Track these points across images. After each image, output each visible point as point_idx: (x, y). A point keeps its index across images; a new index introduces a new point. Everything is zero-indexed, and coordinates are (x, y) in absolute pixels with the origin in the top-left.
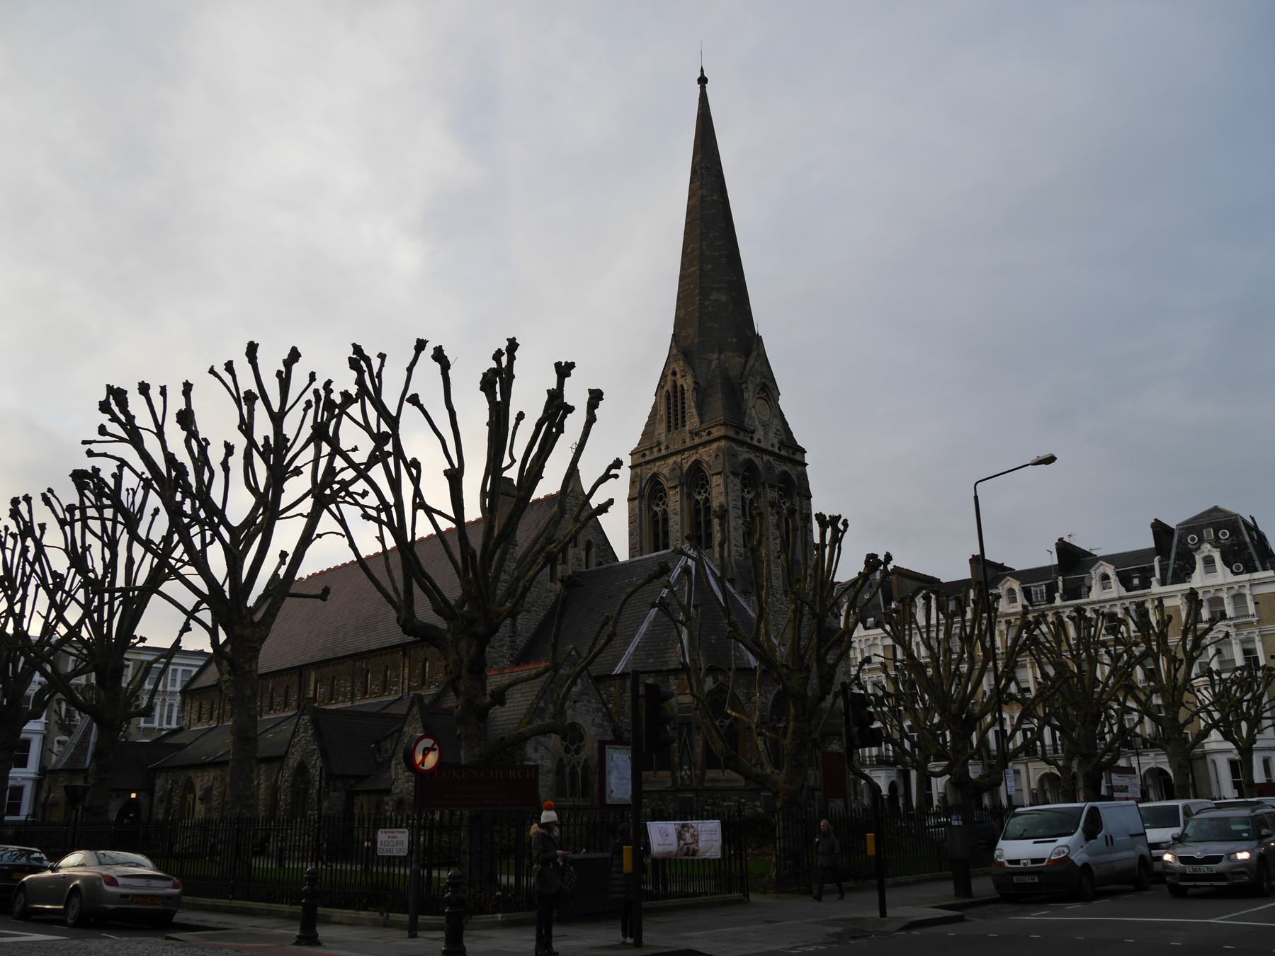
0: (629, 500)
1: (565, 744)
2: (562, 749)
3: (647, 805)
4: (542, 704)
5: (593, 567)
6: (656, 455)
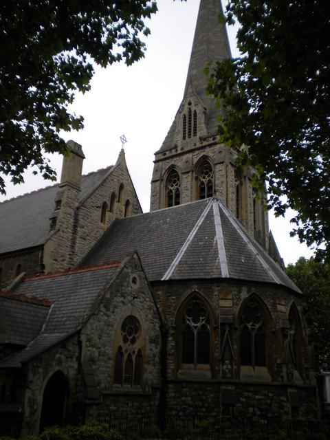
0: (153, 182)
1: (124, 334)
2: (121, 338)
3: (188, 394)
4: (108, 296)
5: (130, 216)
6: (174, 153)
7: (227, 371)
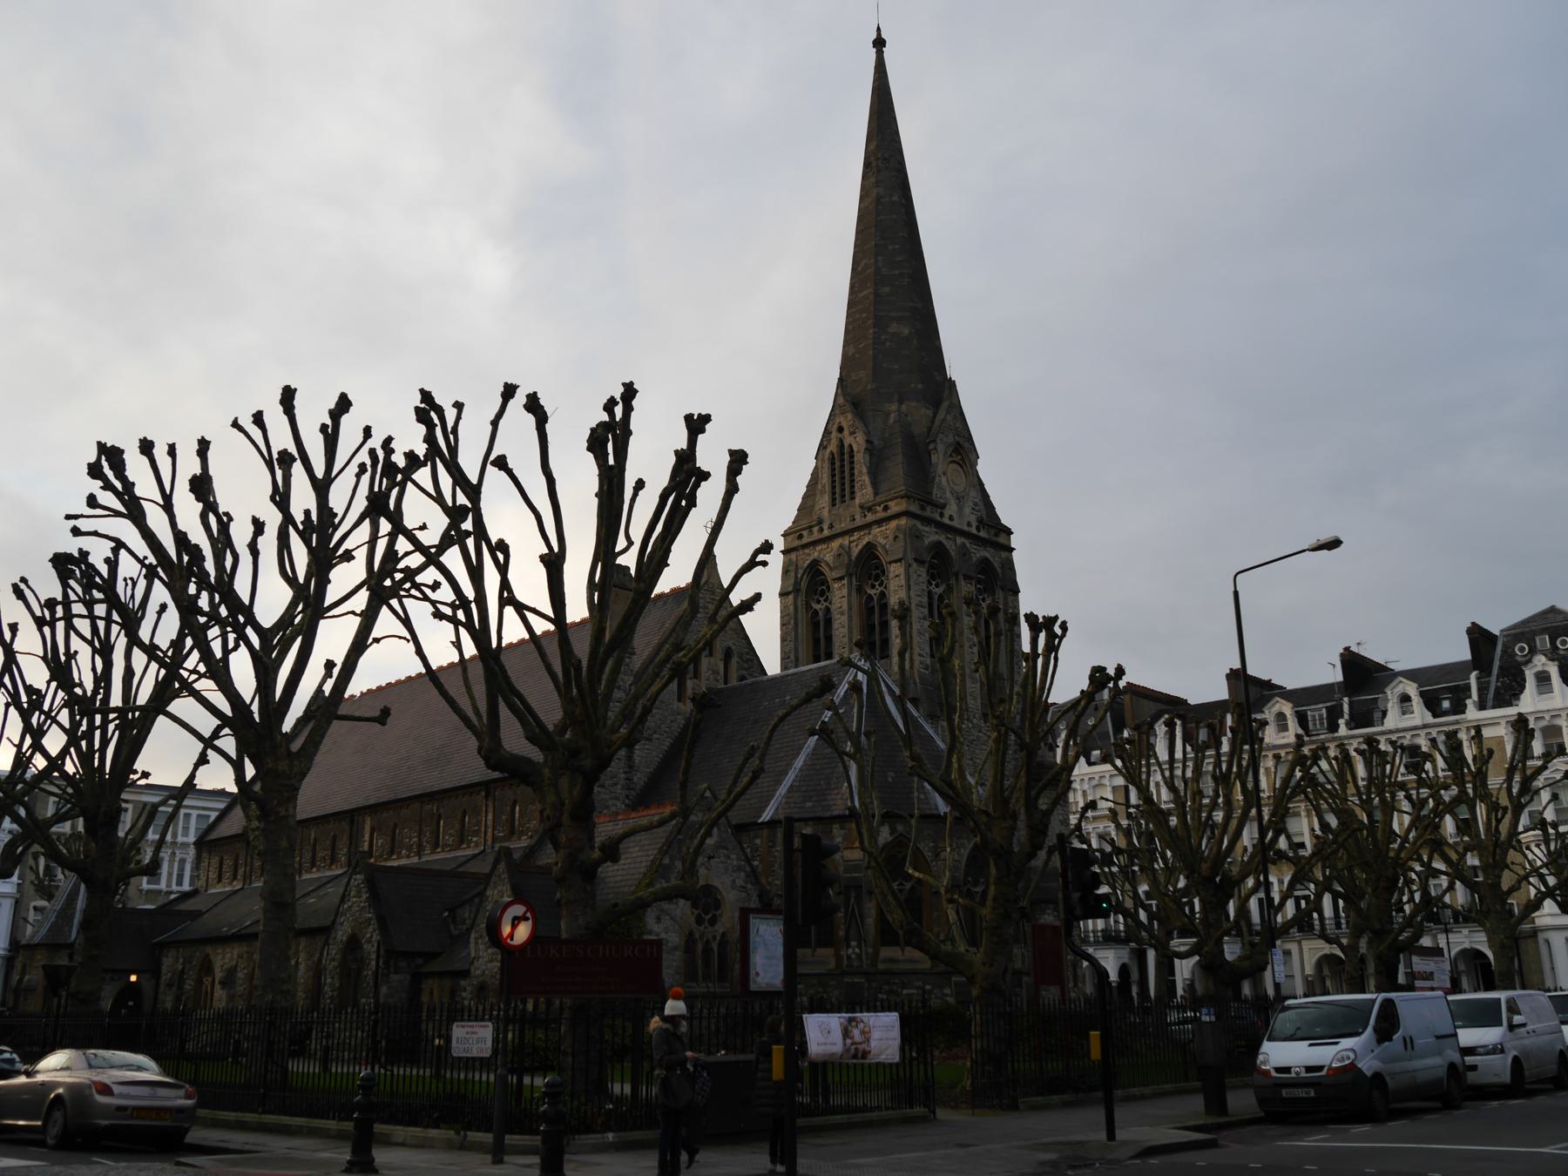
0: (782, 595)
1: (696, 912)
2: (692, 920)
4: (666, 861)
5: (734, 682)
6: (816, 536)
7: (853, 956)
